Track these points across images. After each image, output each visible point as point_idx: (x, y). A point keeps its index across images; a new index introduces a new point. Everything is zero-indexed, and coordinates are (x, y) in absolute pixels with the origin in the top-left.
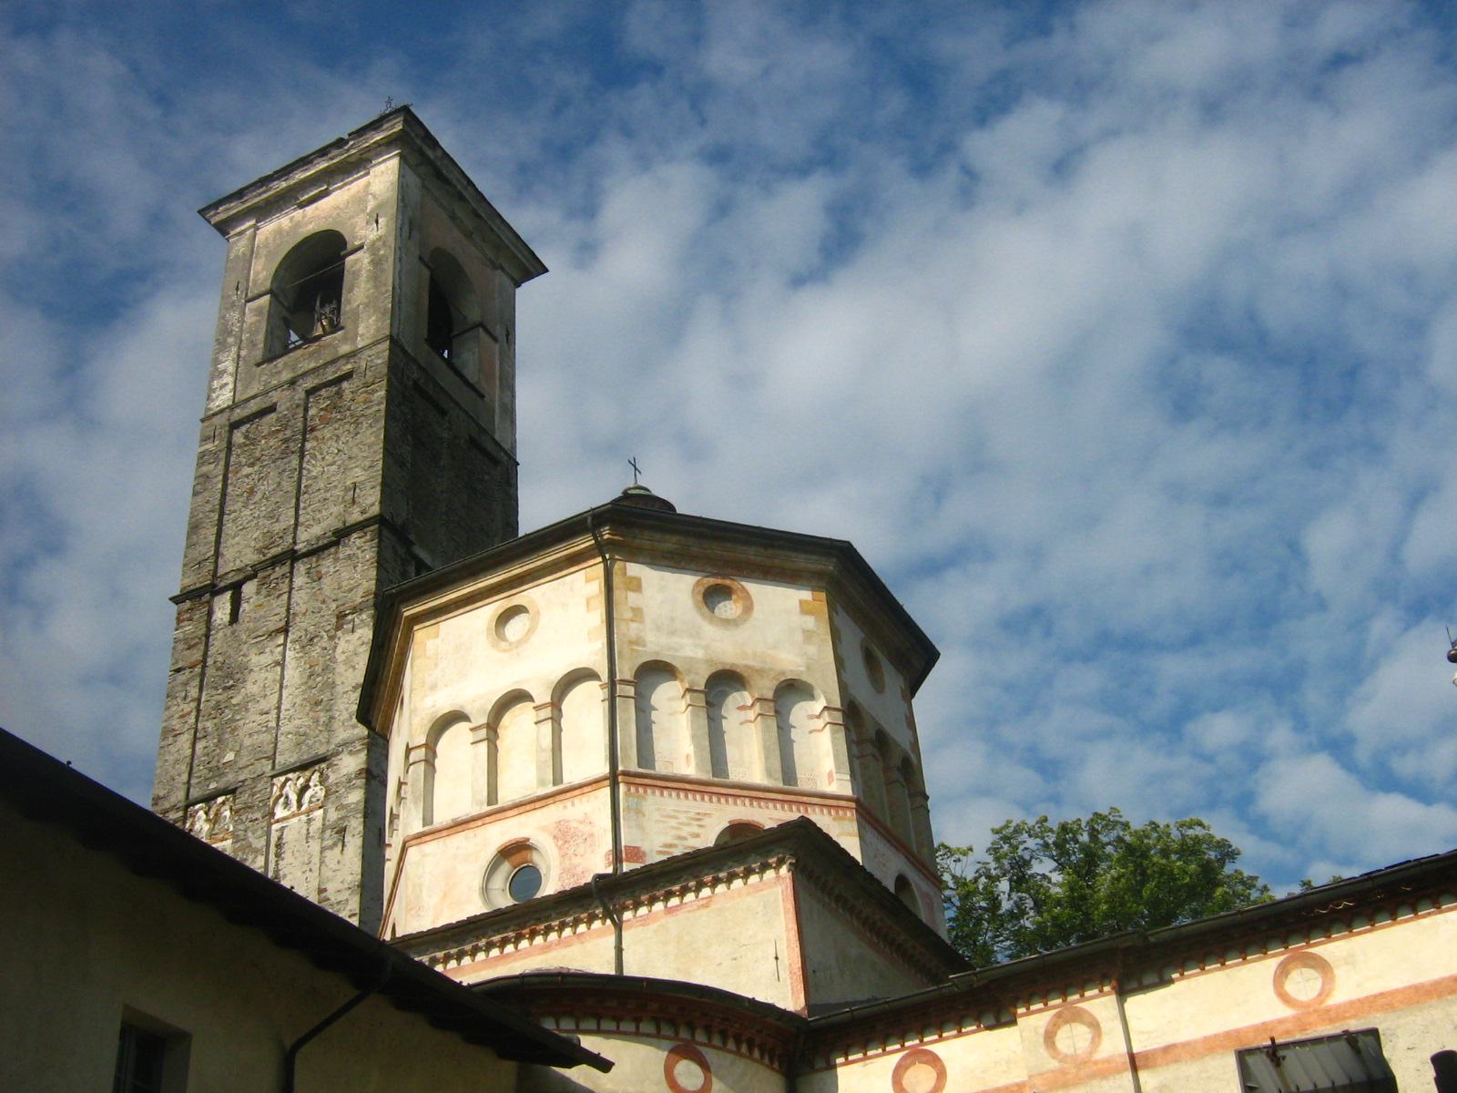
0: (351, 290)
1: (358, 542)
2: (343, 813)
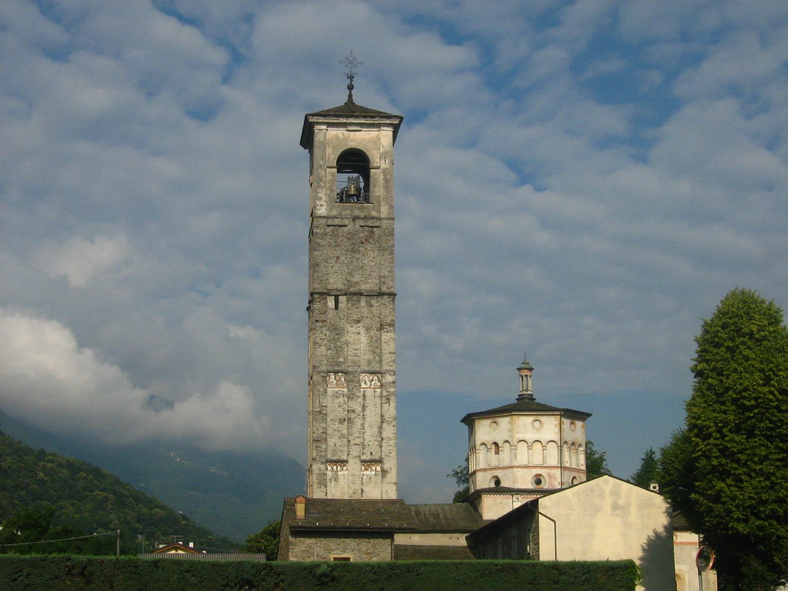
0: (375, 186)
1: (388, 300)
2: (388, 394)
